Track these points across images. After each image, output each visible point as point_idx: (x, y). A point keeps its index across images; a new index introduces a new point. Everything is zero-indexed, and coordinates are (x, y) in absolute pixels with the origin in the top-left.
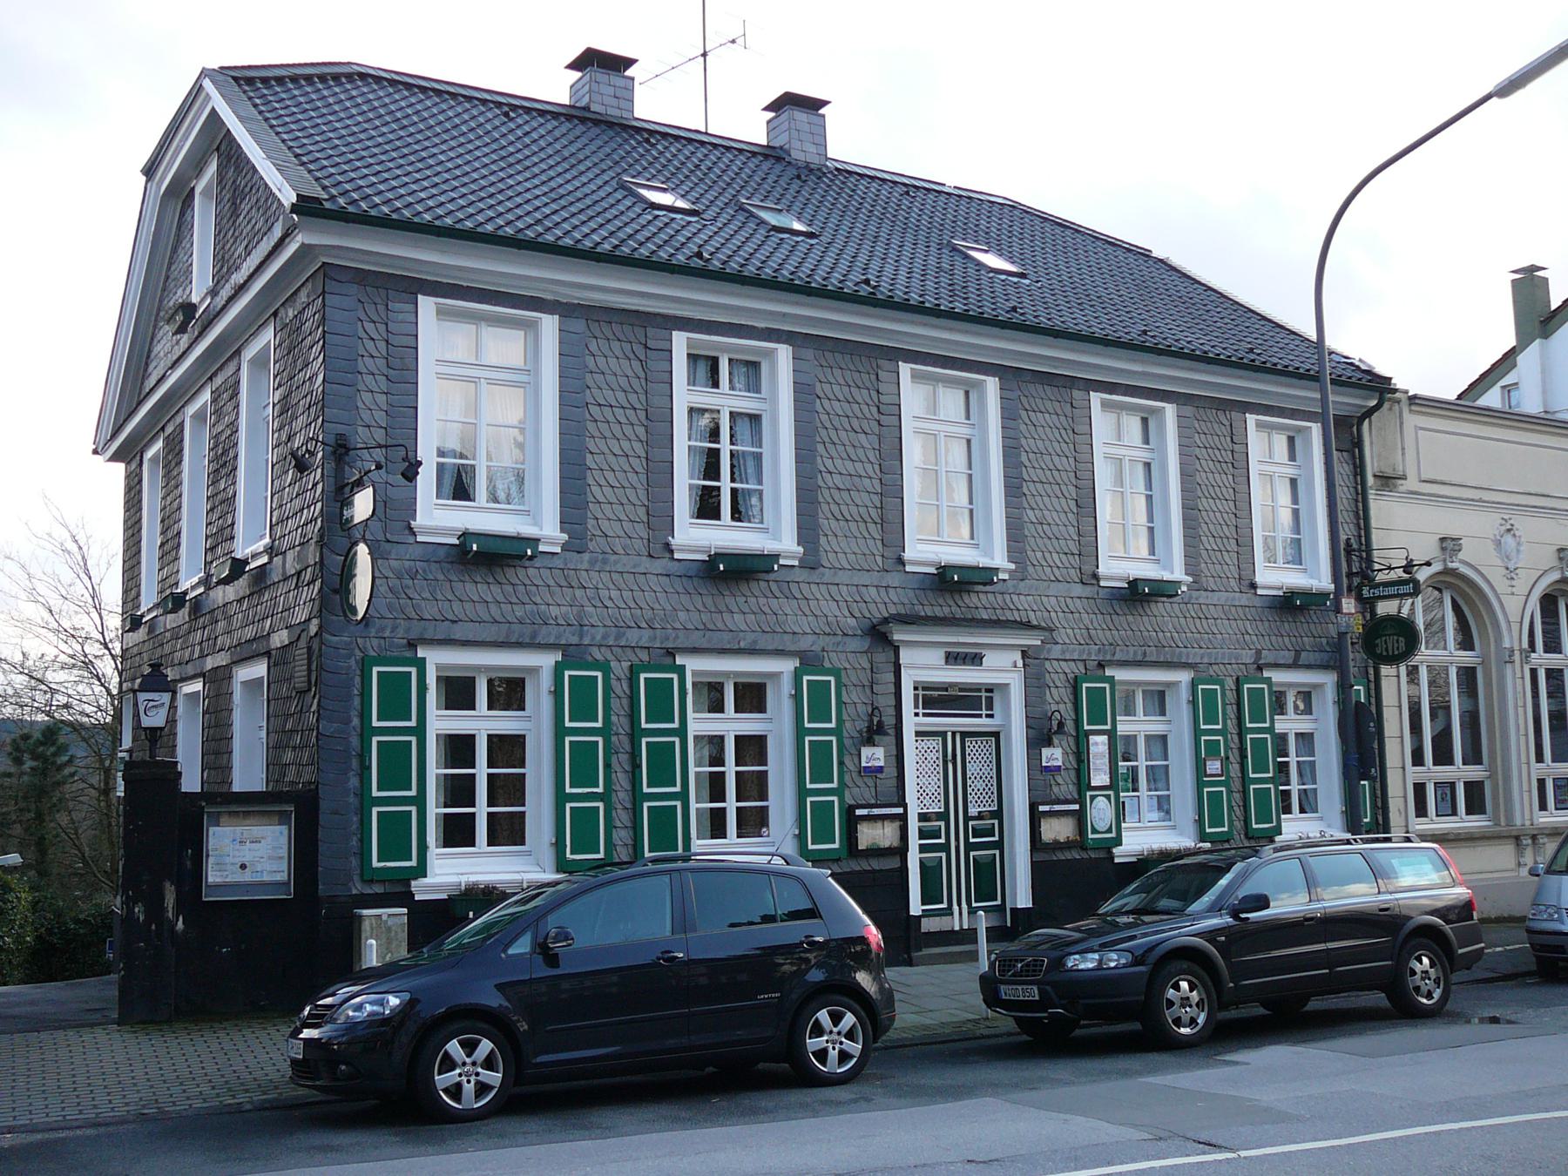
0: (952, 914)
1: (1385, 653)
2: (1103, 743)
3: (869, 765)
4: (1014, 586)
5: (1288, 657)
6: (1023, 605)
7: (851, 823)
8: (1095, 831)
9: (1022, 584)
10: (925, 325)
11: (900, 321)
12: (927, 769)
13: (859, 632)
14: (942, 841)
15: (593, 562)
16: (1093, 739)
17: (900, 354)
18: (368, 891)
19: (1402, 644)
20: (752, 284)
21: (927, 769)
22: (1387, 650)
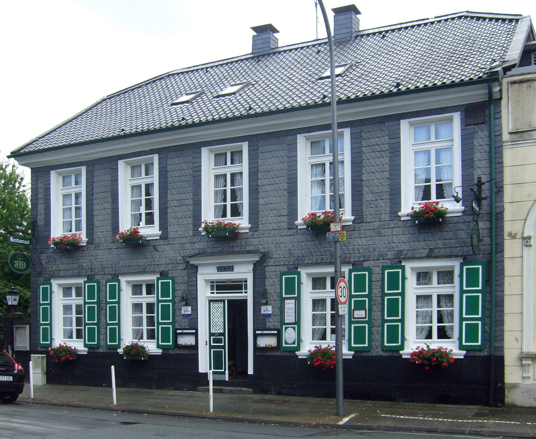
0: (225, 374)
1: (18, 268)
2: (292, 303)
3: (265, 313)
4: (251, 235)
5: (425, 252)
6: (256, 242)
7: (176, 335)
8: (286, 343)
9: (256, 233)
10: (203, 130)
11: (192, 132)
12: (217, 315)
13: (183, 262)
14: (223, 344)
15: (95, 247)
16: (287, 301)
17: (399, 117)
18: (41, 350)
19: (25, 265)
20: (25, 155)
21: (217, 315)
22: (19, 266)
